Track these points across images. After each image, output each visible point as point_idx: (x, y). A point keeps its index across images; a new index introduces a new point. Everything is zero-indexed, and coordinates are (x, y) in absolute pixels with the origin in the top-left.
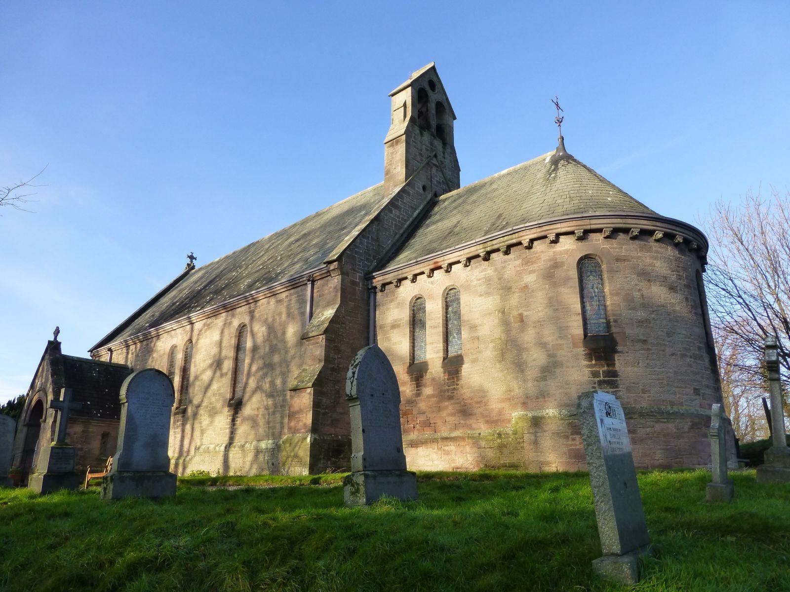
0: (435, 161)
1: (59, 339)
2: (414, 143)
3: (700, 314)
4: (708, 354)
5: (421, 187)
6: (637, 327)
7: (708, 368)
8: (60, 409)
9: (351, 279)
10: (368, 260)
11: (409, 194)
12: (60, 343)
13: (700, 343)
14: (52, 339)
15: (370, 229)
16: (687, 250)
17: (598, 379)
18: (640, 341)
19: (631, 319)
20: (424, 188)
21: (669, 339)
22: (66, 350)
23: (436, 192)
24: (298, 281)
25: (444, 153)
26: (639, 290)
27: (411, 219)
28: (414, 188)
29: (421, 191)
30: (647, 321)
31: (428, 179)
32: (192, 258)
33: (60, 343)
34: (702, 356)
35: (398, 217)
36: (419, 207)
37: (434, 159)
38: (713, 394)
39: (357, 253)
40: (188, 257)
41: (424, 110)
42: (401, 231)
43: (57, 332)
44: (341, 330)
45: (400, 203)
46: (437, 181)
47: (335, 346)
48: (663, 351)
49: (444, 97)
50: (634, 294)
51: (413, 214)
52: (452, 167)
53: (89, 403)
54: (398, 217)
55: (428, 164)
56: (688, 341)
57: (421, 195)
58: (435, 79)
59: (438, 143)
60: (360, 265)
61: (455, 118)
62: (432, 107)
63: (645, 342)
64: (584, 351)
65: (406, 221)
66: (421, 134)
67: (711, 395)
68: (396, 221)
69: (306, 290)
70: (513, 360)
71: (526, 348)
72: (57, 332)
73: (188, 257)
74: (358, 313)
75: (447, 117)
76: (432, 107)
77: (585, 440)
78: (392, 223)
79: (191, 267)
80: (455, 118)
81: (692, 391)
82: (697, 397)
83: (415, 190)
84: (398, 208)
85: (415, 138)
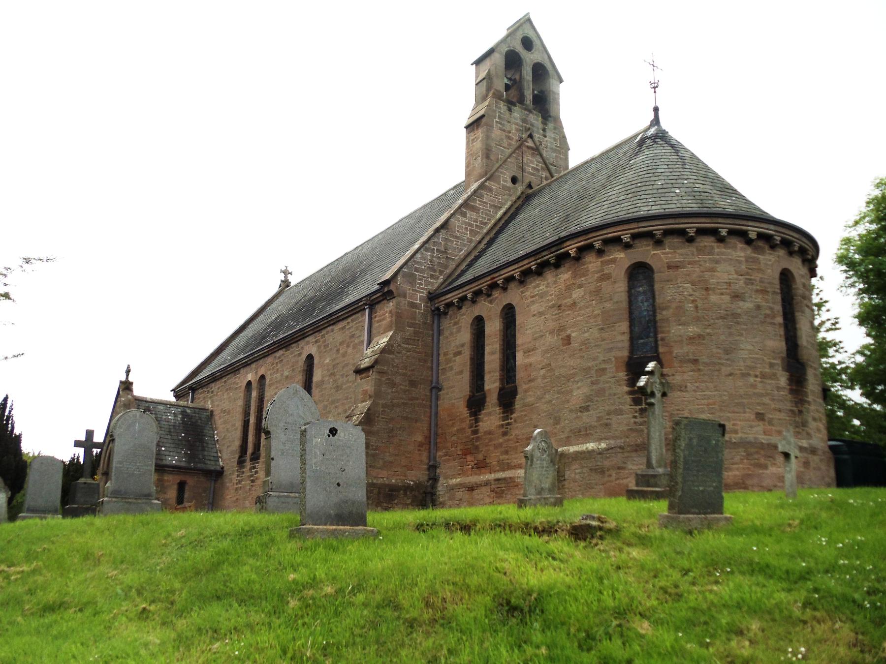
0: (530, 143)
1: (130, 379)
2: (499, 125)
3: (780, 324)
4: (787, 371)
5: (509, 180)
6: (688, 345)
7: (785, 388)
8: (812, 323)
9: (409, 302)
10: (432, 276)
11: (491, 190)
12: (131, 384)
13: (774, 359)
14: (124, 379)
15: (436, 240)
16: (767, 247)
17: (640, 407)
18: (689, 361)
19: (680, 336)
20: (514, 180)
21: (727, 357)
22: (138, 391)
23: (530, 182)
24: (356, 306)
25: (544, 130)
26: (693, 301)
27: (493, 222)
28: (499, 183)
29: (509, 184)
30: (700, 336)
31: (520, 167)
32: (286, 272)
33: (131, 384)
34: (775, 375)
35: (476, 221)
36: (505, 204)
37: (529, 140)
38: (787, 418)
39: (417, 270)
40: (282, 271)
41: (517, 77)
42: (478, 238)
43: (128, 372)
44: (396, 361)
45: (477, 204)
46: (533, 168)
47: (389, 379)
48: (718, 371)
49: (546, 57)
50: (686, 306)
51: (496, 213)
52: (556, 146)
53: (163, 449)
54: (476, 221)
55: (519, 147)
56: (753, 358)
57: (509, 189)
58: (531, 34)
59: (535, 120)
60: (421, 284)
61: (561, 81)
62: (527, 73)
63: (695, 361)
64: (627, 375)
65: (486, 224)
66: (510, 110)
67: (785, 419)
68: (471, 225)
69: (364, 314)
70: (206, 453)
71: (855, 318)
72: (128, 372)
73: (282, 271)
74: (418, 340)
75: (553, 81)
76: (527, 73)
77: (162, 527)
78: (466, 229)
79: (285, 284)
80: (561, 81)
81: (753, 417)
82: (761, 423)
83: (499, 184)
84: (474, 209)
85: (500, 118)
